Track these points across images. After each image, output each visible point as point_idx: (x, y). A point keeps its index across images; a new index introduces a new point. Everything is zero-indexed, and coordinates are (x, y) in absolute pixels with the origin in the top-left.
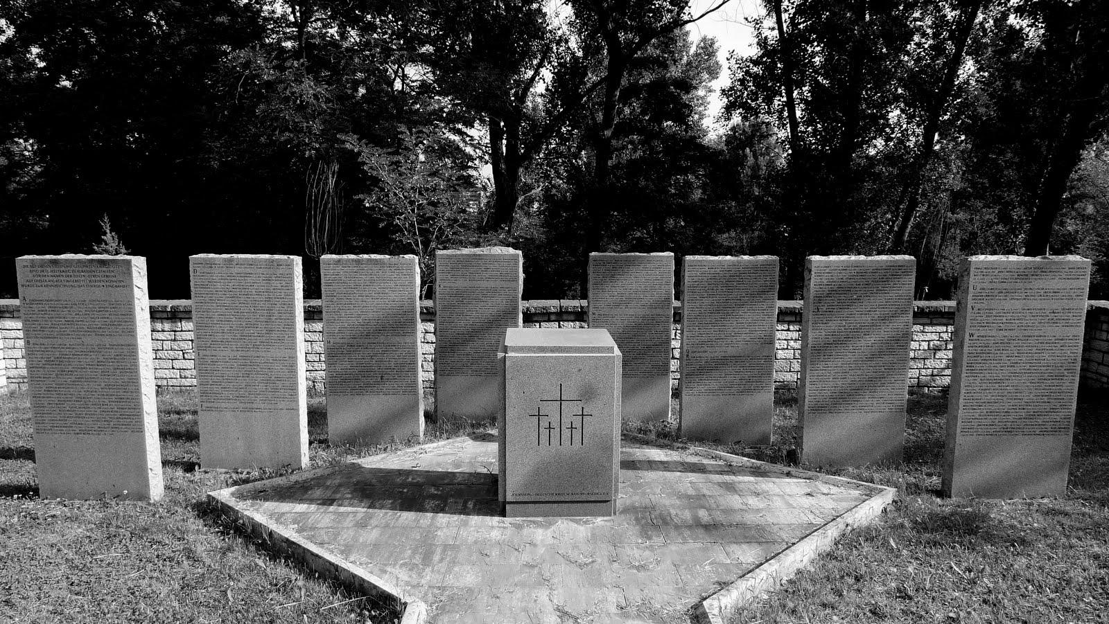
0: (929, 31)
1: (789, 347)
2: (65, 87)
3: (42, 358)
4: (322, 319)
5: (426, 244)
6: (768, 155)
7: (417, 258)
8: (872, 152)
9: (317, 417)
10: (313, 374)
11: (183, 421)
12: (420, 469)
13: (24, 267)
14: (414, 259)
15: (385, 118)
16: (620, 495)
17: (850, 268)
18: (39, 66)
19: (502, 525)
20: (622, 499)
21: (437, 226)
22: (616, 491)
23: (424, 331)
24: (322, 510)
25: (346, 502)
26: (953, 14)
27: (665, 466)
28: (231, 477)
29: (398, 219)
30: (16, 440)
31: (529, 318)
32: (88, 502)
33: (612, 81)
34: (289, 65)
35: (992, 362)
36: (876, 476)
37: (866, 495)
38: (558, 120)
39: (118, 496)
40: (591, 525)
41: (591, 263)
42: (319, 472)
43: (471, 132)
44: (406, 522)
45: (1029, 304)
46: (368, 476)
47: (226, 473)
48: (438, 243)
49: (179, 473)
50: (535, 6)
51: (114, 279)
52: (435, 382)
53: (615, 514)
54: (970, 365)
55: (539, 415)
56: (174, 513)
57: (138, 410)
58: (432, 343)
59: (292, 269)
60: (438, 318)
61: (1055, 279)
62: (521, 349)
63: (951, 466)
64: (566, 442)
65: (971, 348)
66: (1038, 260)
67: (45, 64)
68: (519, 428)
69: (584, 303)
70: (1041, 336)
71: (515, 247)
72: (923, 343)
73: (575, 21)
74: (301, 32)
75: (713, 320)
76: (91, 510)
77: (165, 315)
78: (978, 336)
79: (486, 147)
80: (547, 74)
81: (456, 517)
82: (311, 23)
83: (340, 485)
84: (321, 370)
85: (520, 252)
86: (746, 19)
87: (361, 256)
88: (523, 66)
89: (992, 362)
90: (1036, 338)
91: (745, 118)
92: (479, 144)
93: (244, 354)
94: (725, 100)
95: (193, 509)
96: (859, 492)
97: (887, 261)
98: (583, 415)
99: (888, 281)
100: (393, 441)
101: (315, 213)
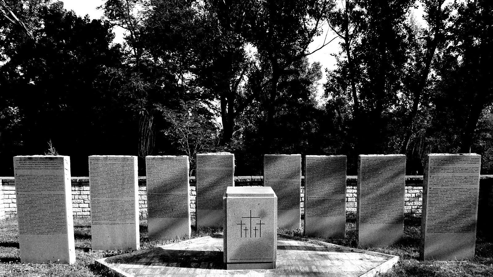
0: (414, 58)
1: (353, 197)
2: (31, 84)
3: (23, 200)
4: (146, 185)
5: (192, 152)
6: (345, 112)
7: (188, 157)
8: (391, 111)
9: (143, 229)
10: (142, 210)
11: (84, 230)
12: (189, 250)
13: (17, 160)
14: (186, 158)
15: (175, 97)
16: (277, 260)
17: (377, 160)
18: (21, 75)
19: (225, 273)
20: (278, 262)
21: (197, 144)
22: (276, 258)
23: (191, 190)
24: (146, 267)
25: (157, 264)
26: (425, 50)
27: (298, 248)
28: (105, 254)
29: (180, 141)
30: (9, 239)
31: (238, 184)
32: (42, 265)
33: (274, 80)
34: (133, 74)
35: (440, 200)
36: (391, 252)
37: (386, 259)
38: (250, 98)
39: (55, 262)
40: (264, 273)
41: (265, 159)
42: (144, 251)
43: (212, 102)
44: (183, 272)
45: (459, 176)
46: (166, 253)
47: (103, 252)
48: (197, 151)
49: (82, 252)
50: (241, 48)
51: (56, 166)
52: (196, 212)
53: (275, 268)
54: (430, 202)
55: (241, 224)
56: (80, 269)
57: (65, 224)
58: (195, 195)
59: (133, 161)
60: (197, 184)
61: (465, 163)
62: (233, 195)
63: (423, 247)
64: (253, 236)
65: (430, 194)
66: (458, 155)
67: (23, 74)
68: (233, 230)
69: (262, 177)
70: (460, 189)
71: (232, 152)
72: (413, 194)
73: (258, 54)
74: (138, 59)
76: (43, 268)
77: (76, 184)
78: (433, 189)
79: (219, 109)
80: (246, 78)
81: (205, 270)
82: (142, 55)
83: (154, 257)
84: (145, 208)
85: (233, 154)
86: (331, 55)
87: (164, 156)
88: (236, 74)
89: (440, 200)
90: (458, 189)
91: (334, 96)
92: (216, 108)
93: (112, 199)
94: (325, 89)
95: (88, 267)
96: (383, 258)
97: (393, 157)
98: (260, 224)
99: (394, 165)
100: (177, 238)
101: (143, 138)
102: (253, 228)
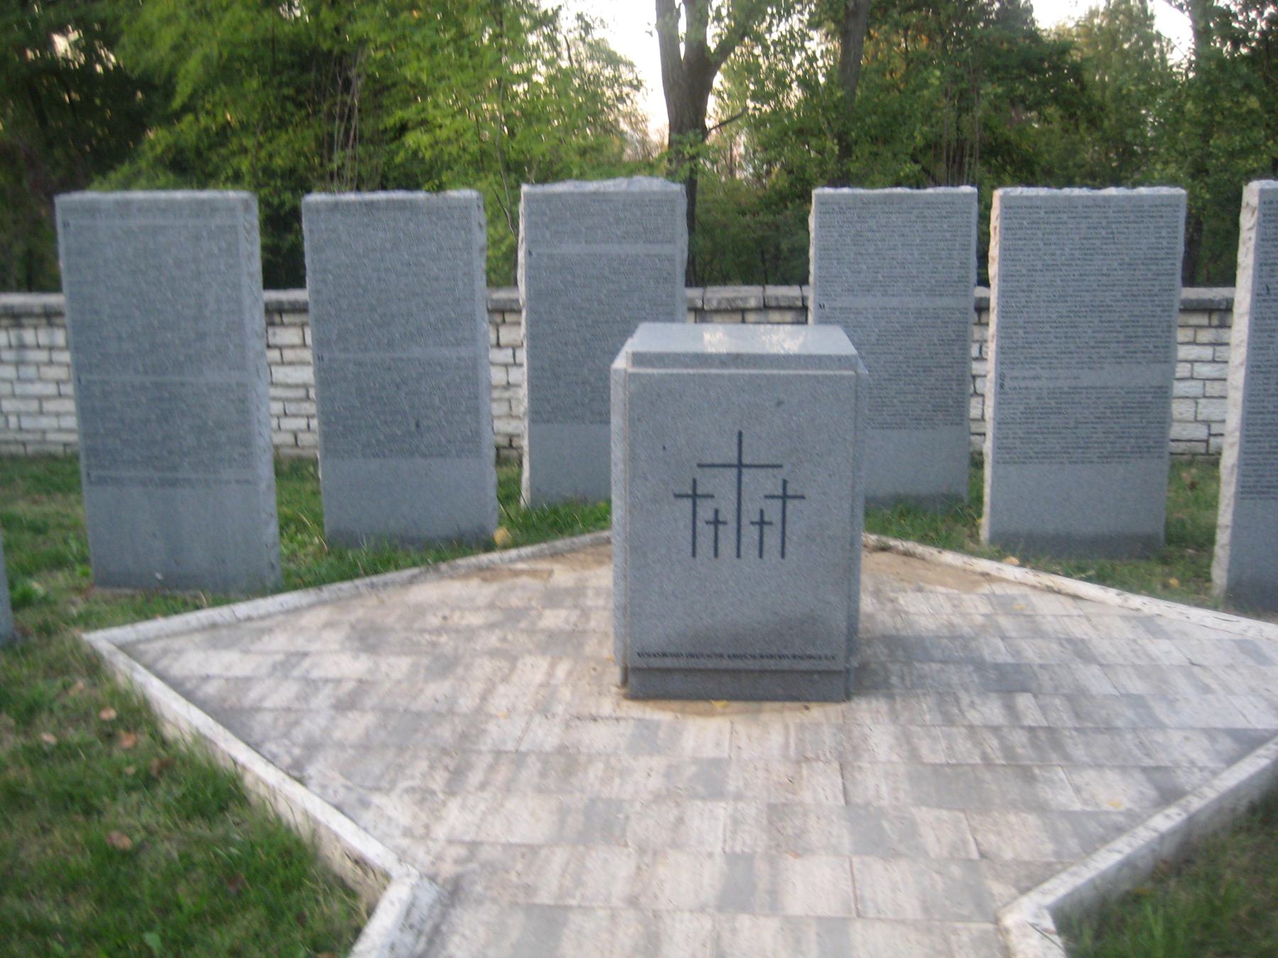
14: (531, 198)
75: (1054, 316)
98: (740, 466)
102: (751, 513)
